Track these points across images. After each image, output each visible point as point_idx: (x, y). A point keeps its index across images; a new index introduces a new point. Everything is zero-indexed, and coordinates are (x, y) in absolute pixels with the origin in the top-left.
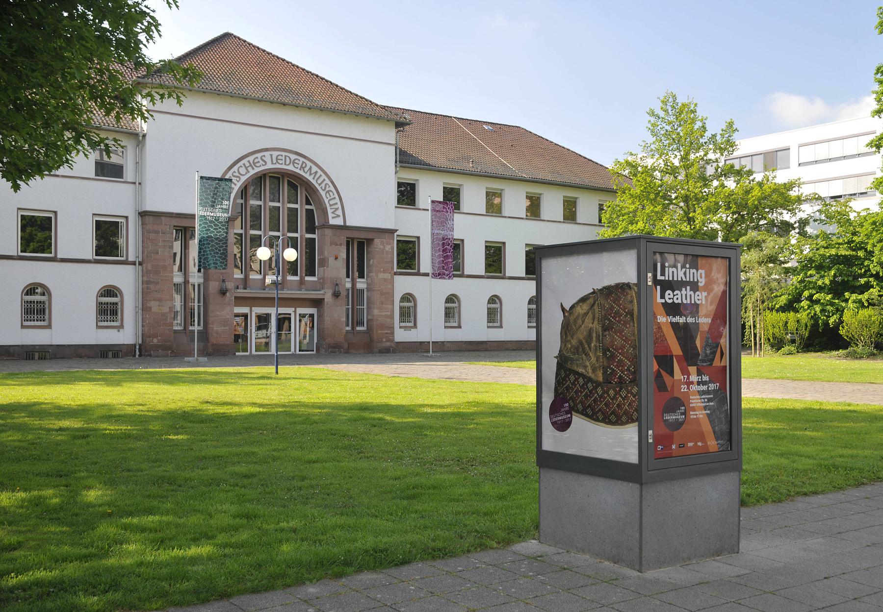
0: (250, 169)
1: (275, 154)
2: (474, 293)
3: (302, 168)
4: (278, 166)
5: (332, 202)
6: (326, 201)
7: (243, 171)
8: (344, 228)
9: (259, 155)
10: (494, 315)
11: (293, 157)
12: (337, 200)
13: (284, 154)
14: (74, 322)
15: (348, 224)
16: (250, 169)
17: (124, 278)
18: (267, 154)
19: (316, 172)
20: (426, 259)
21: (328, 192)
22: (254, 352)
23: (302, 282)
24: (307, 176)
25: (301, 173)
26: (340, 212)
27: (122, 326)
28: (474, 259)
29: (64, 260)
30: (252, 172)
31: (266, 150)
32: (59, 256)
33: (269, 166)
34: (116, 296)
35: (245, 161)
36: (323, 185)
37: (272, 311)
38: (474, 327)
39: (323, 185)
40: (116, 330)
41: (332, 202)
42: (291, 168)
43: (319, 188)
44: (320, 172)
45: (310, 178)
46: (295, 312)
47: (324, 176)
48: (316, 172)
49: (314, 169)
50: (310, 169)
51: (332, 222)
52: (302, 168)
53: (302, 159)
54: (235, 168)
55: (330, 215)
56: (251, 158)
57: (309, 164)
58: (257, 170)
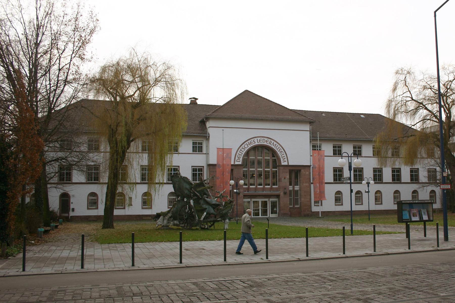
1: (259, 139)
6: (280, 156)
7: (246, 146)
9: (252, 140)
11: (266, 139)
12: (285, 155)
13: (262, 138)
18: (256, 139)
25: (270, 145)
26: (286, 160)
30: (250, 146)
33: (257, 143)
35: (247, 142)
36: (279, 149)
38: (369, 204)
39: (279, 149)
42: (265, 143)
43: (277, 151)
45: (273, 147)
47: (279, 146)
49: (275, 143)
51: (283, 164)
53: (270, 140)
54: (243, 146)
55: (282, 161)
56: (249, 141)
57: (273, 141)
58: (252, 145)
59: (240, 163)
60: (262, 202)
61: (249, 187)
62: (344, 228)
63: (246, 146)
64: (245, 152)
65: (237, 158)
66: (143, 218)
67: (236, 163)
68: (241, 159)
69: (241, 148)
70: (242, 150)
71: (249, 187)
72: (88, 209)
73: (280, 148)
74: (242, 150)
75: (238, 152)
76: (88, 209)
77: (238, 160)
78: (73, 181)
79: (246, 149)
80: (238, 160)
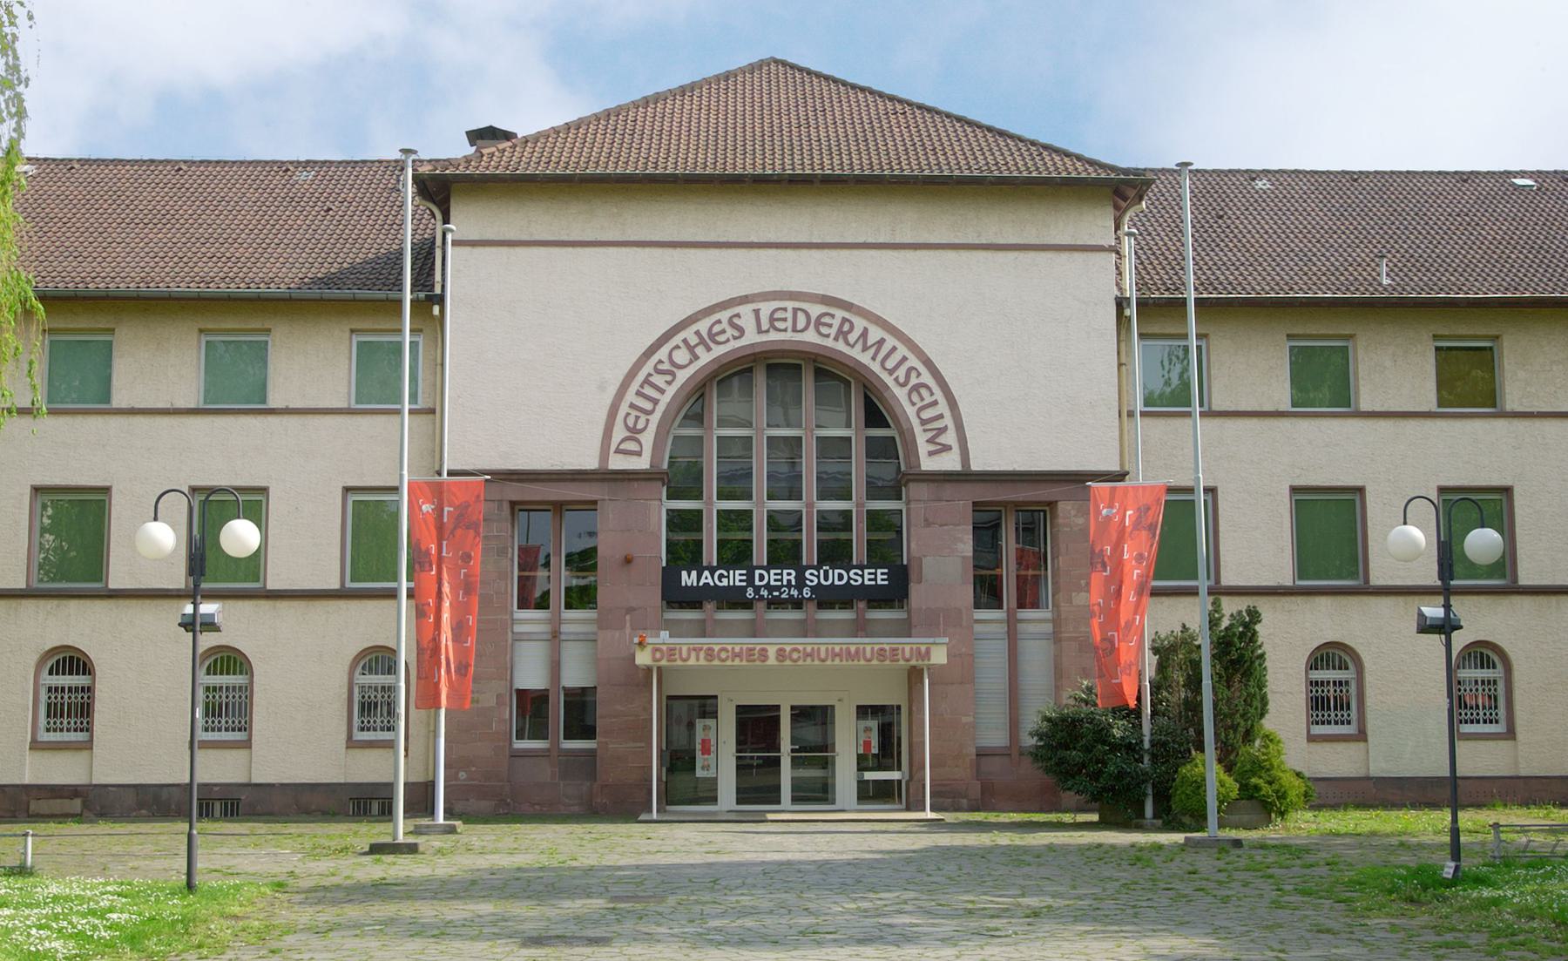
1: (766, 308)
4: (773, 336)
7: (681, 356)
11: (816, 310)
18: (746, 310)
24: (856, 353)
30: (705, 358)
31: (745, 300)
33: (751, 338)
35: (689, 334)
44: (891, 341)
45: (865, 359)
47: (902, 350)
49: (875, 334)
51: (928, 464)
54: (662, 354)
55: (923, 448)
56: (703, 326)
57: (860, 323)
58: (718, 351)
59: (642, 463)
63: (681, 356)
64: (671, 391)
65: (619, 433)
67: (617, 463)
68: (647, 439)
69: (648, 367)
70: (659, 380)
74: (659, 380)
75: (630, 396)
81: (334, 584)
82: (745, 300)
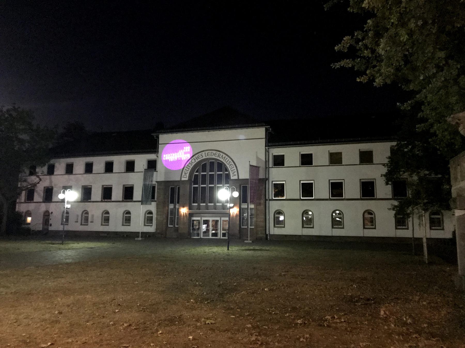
0: (196, 160)
1: (207, 152)
2: (116, 210)
3: (219, 156)
5: (232, 169)
6: (189, 172)
7: (193, 161)
8: (238, 179)
10: (127, 220)
11: (214, 152)
12: (235, 168)
13: (211, 151)
14: (138, 225)
15: (240, 178)
16: (196, 160)
17: (152, 207)
18: (203, 153)
19: (225, 157)
20: (138, 194)
21: (230, 165)
22: (202, 237)
23: (207, 205)
26: (236, 173)
27: (408, 229)
28: (117, 194)
29: (93, 202)
30: (197, 161)
31: (203, 151)
32: (378, 197)
33: (204, 157)
34: (439, 215)
36: (228, 162)
37: (211, 219)
38: (116, 225)
39: (228, 162)
40: (150, 227)
41: (232, 169)
44: (227, 157)
46: (221, 219)
47: (229, 158)
48: (225, 157)
49: (224, 156)
50: (222, 156)
52: (219, 156)
53: (218, 152)
54: (233, 164)
56: (197, 156)
57: (222, 154)
59: (187, 179)
60: (213, 221)
61: (207, 204)
62: (228, 249)
65: (183, 174)
66: (106, 235)
67: (183, 179)
68: (188, 175)
70: (189, 165)
71: (207, 204)
72: (145, 225)
73: (230, 160)
74: (189, 165)
76: (145, 225)
77: (185, 176)
78: (92, 200)
79: (193, 164)
80: (185, 176)
81: (359, 197)
82: (203, 151)
